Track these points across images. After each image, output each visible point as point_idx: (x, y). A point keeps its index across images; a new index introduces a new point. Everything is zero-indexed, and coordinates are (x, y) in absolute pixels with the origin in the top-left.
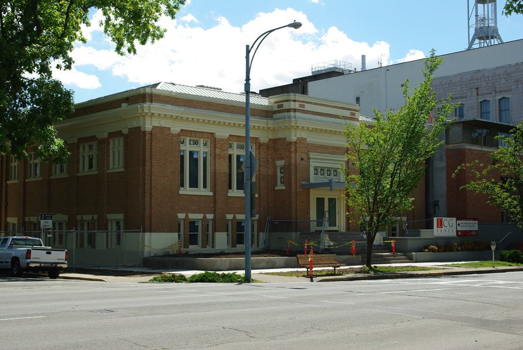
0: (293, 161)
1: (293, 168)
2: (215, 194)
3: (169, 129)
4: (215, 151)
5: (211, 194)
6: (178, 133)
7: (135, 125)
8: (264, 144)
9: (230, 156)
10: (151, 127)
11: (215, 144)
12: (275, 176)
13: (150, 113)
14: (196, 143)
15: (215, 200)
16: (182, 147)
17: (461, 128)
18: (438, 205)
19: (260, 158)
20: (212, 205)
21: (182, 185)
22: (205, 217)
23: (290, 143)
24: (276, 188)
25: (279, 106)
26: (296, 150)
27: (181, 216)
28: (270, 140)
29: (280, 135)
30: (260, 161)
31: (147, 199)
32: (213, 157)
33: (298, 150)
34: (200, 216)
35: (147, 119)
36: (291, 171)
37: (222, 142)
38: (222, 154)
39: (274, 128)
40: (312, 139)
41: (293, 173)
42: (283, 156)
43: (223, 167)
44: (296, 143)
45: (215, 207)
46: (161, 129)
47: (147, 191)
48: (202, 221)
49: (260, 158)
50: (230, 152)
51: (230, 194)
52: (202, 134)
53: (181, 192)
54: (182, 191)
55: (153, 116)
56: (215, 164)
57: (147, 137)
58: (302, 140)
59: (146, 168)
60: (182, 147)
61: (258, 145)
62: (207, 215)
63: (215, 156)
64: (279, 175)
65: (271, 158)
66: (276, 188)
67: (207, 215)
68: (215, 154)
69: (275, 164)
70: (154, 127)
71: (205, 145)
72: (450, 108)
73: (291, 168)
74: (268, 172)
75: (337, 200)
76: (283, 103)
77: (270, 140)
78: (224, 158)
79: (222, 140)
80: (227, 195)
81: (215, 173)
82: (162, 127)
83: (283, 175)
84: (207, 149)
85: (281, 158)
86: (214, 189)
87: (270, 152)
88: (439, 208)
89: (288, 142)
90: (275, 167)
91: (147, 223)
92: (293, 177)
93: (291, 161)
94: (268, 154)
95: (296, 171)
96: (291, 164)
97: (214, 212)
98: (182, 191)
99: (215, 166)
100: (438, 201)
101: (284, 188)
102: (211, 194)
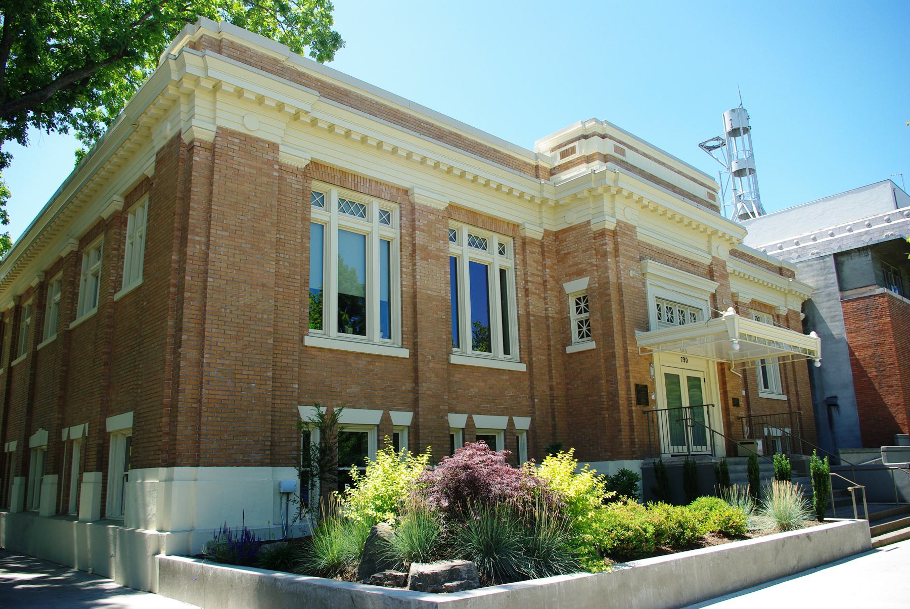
0: (612, 278)
1: (613, 292)
2: (414, 354)
3: (274, 147)
4: (414, 238)
5: (405, 353)
6: (302, 166)
7: (168, 132)
8: (533, 241)
9: (454, 261)
10: (215, 129)
11: (413, 220)
12: (565, 321)
13: (208, 77)
14: (361, 211)
15: (416, 370)
16: (317, 214)
17: (869, 258)
18: (836, 405)
19: (526, 274)
20: (409, 386)
21: (318, 323)
22: (386, 419)
23: (602, 233)
24: (570, 350)
25: (564, 155)
26: (616, 250)
27: (308, 413)
28: (547, 233)
29: (574, 218)
30: (527, 282)
31: (189, 353)
32: (408, 251)
33: (621, 248)
34: (373, 417)
35: (197, 101)
36: (610, 301)
37: (431, 217)
38: (432, 247)
39: (557, 202)
40: (650, 231)
41: (614, 306)
42: (583, 266)
43: (434, 282)
44: (614, 233)
45: (415, 391)
46: (248, 143)
47: (189, 323)
48: (378, 431)
49: (526, 274)
50: (454, 249)
51: (454, 359)
52: (376, 188)
53: (309, 341)
54: (313, 339)
55: (219, 95)
56: (414, 271)
57: (200, 157)
58: (624, 231)
59: (190, 251)
60: (317, 214)
61: (519, 242)
62: (393, 414)
63: (414, 251)
64: (574, 318)
65: (551, 276)
66: (570, 350)
67: (393, 414)
68: (414, 245)
69: (561, 291)
70: (222, 132)
71: (385, 217)
72: (361, 488)
73: (609, 295)
74: (546, 309)
75: (634, 402)
76: (576, 144)
77: (547, 233)
78: (438, 258)
79: (432, 211)
80: (448, 359)
81: (414, 296)
82: (251, 137)
83: (584, 316)
84: (392, 232)
85: (580, 274)
86: (412, 339)
87: (548, 262)
88: (838, 411)
89: (594, 233)
90: (562, 296)
91: (184, 430)
92: (616, 316)
93: (608, 277)
94: (544, 266)
95: (621, 302)
96: (608, 283)
97: (414, 406)
98: (313, 339)
99: (414, 277)
100: (836, 397)
101: (591, 345)
102: (405, 353)
